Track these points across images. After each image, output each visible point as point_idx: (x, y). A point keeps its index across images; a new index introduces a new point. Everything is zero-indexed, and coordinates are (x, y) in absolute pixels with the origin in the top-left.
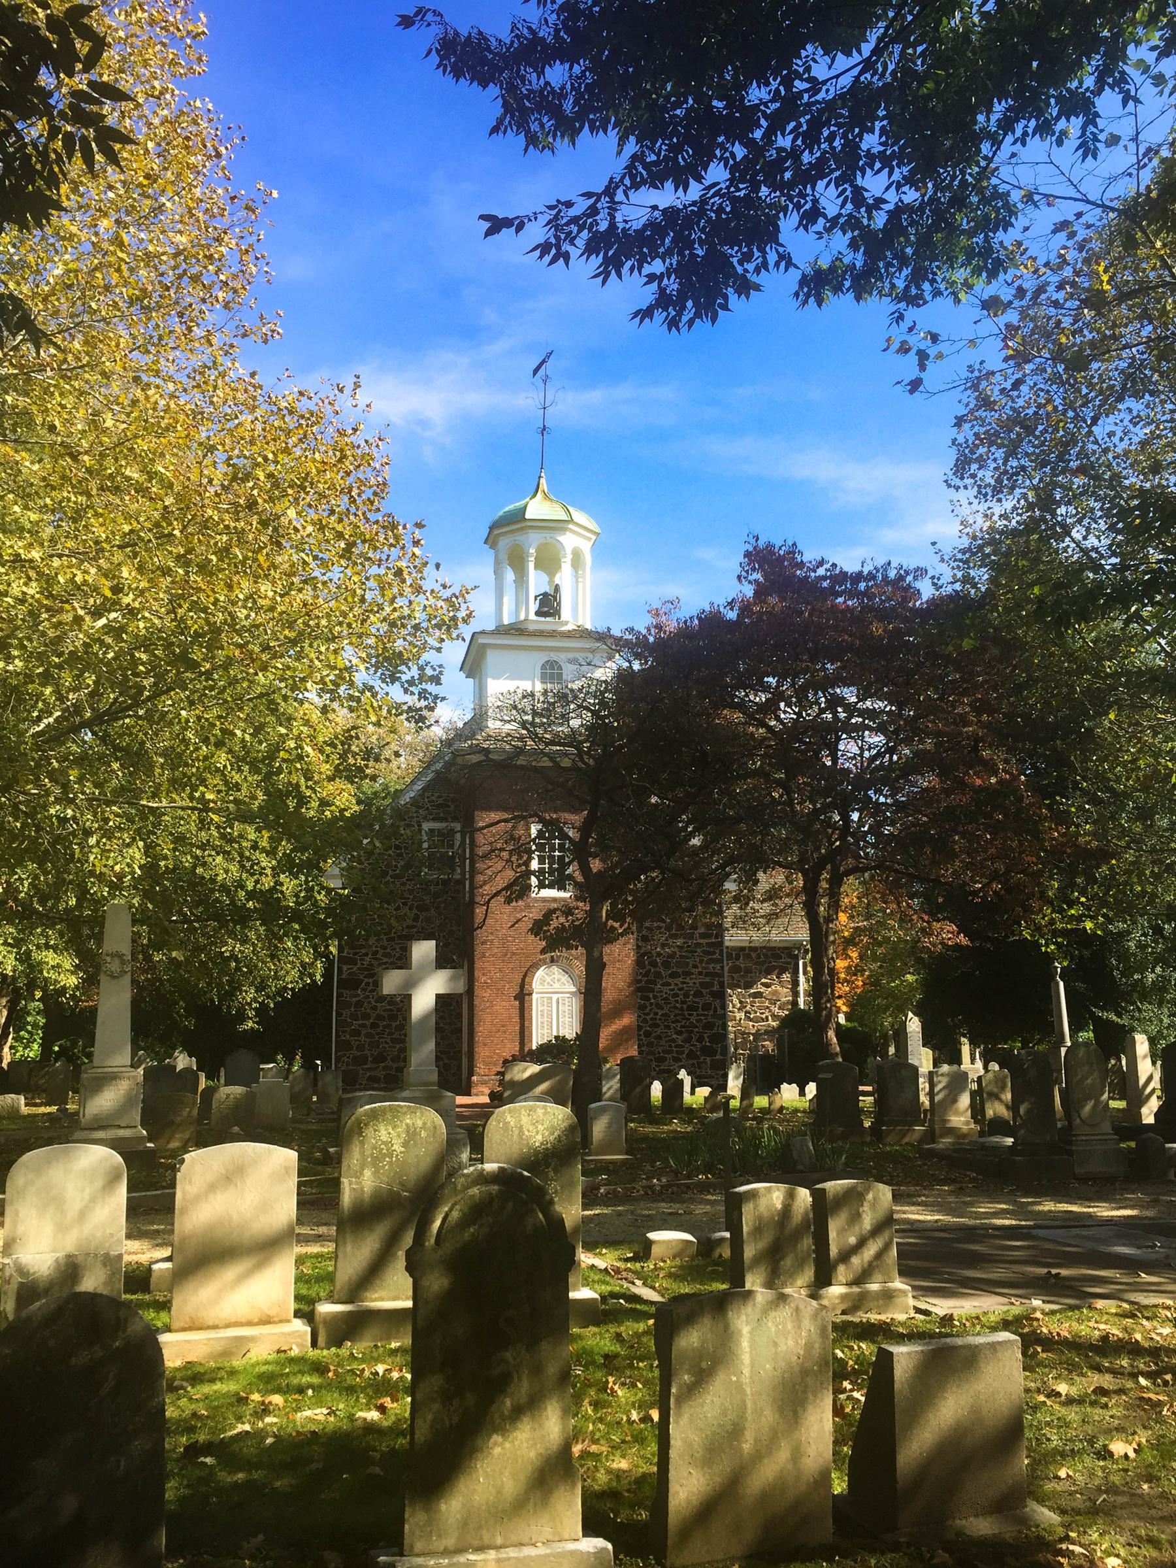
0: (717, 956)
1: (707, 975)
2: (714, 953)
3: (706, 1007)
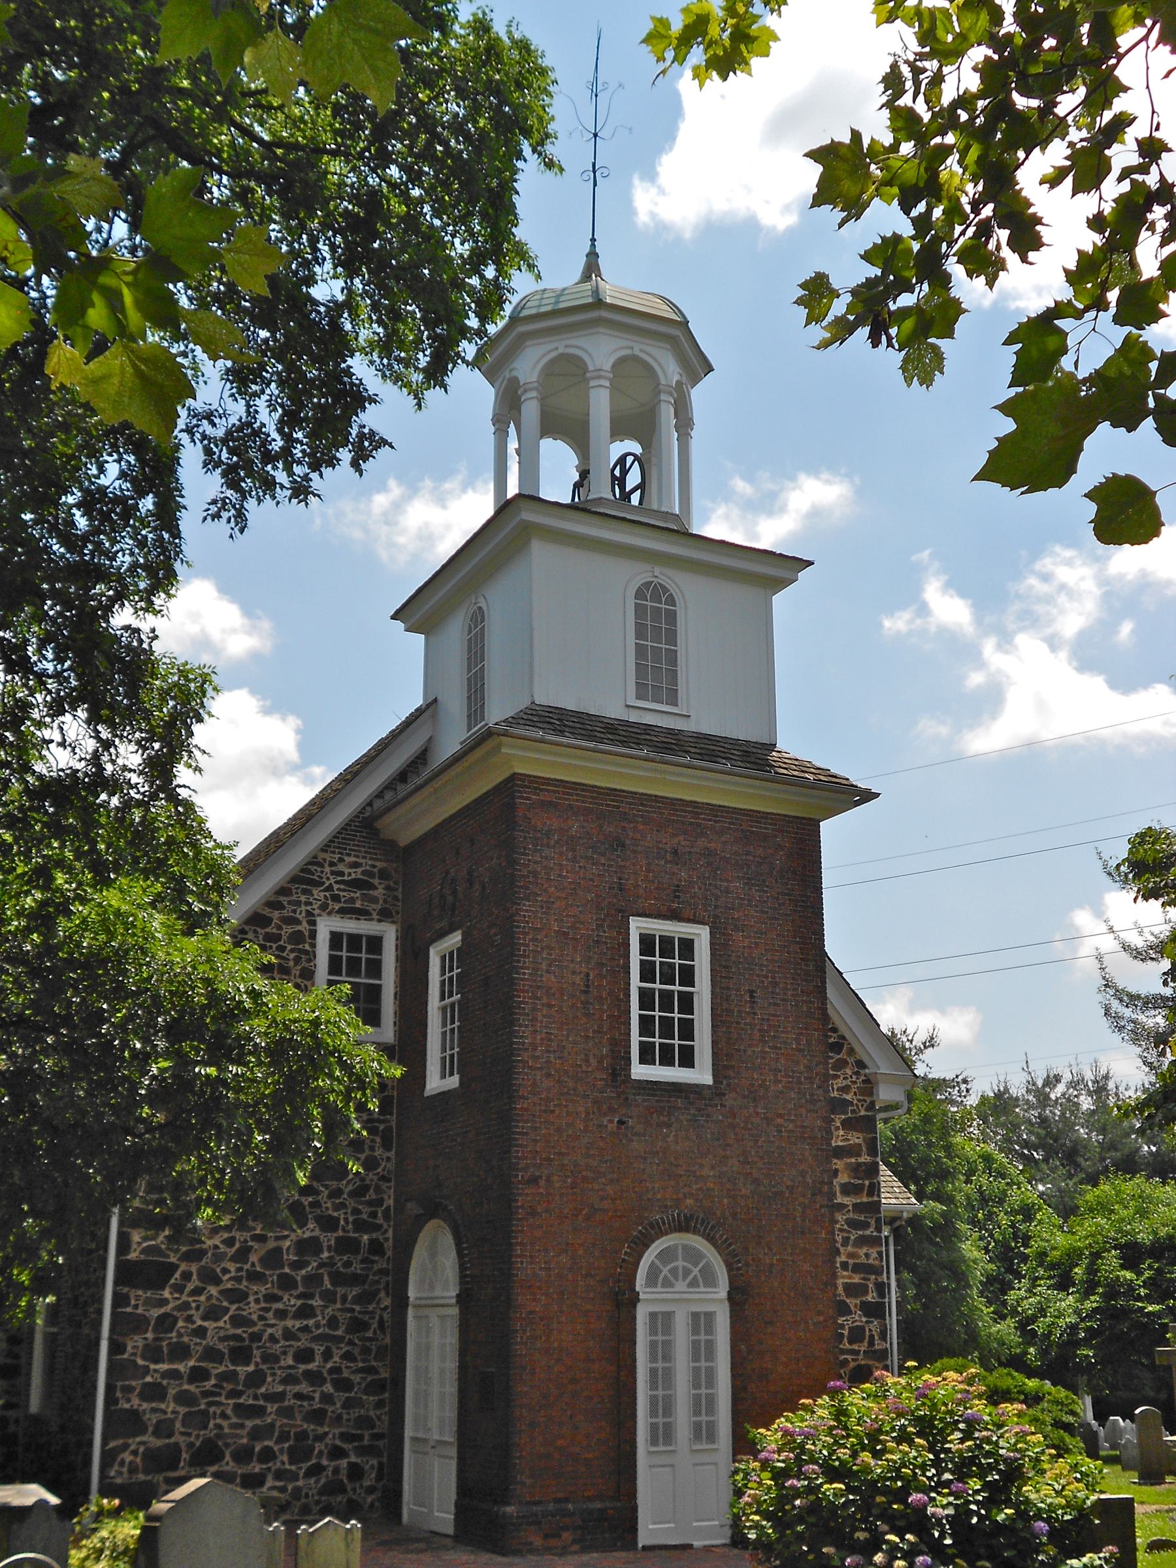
1: (857, 1269)
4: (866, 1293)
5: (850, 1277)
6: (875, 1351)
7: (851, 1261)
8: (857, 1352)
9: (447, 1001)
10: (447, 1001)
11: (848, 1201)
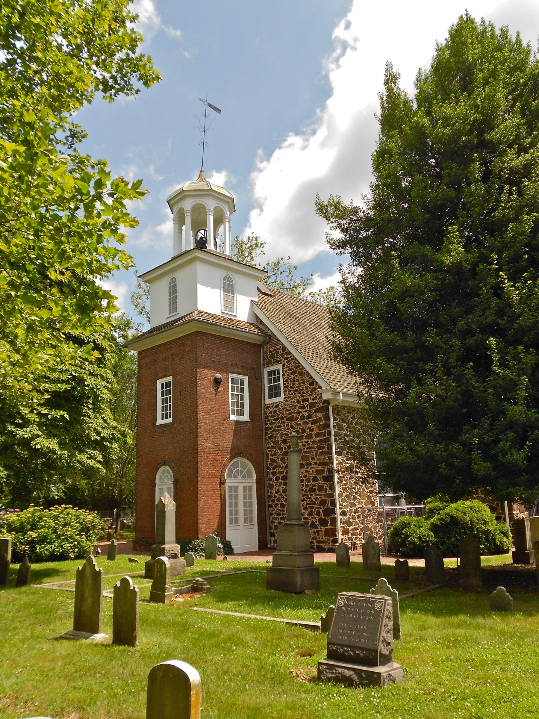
0: (326, 449)
1: (320, 464)
2: (323, 447)
3: (321, 488)
4: (324, 473)
5: (318, 467)
6: (327, 494)
7: (318, 462)
8: (321, 495)
9: (164, 397)
10: (164, 397)
11: (317, 439)
